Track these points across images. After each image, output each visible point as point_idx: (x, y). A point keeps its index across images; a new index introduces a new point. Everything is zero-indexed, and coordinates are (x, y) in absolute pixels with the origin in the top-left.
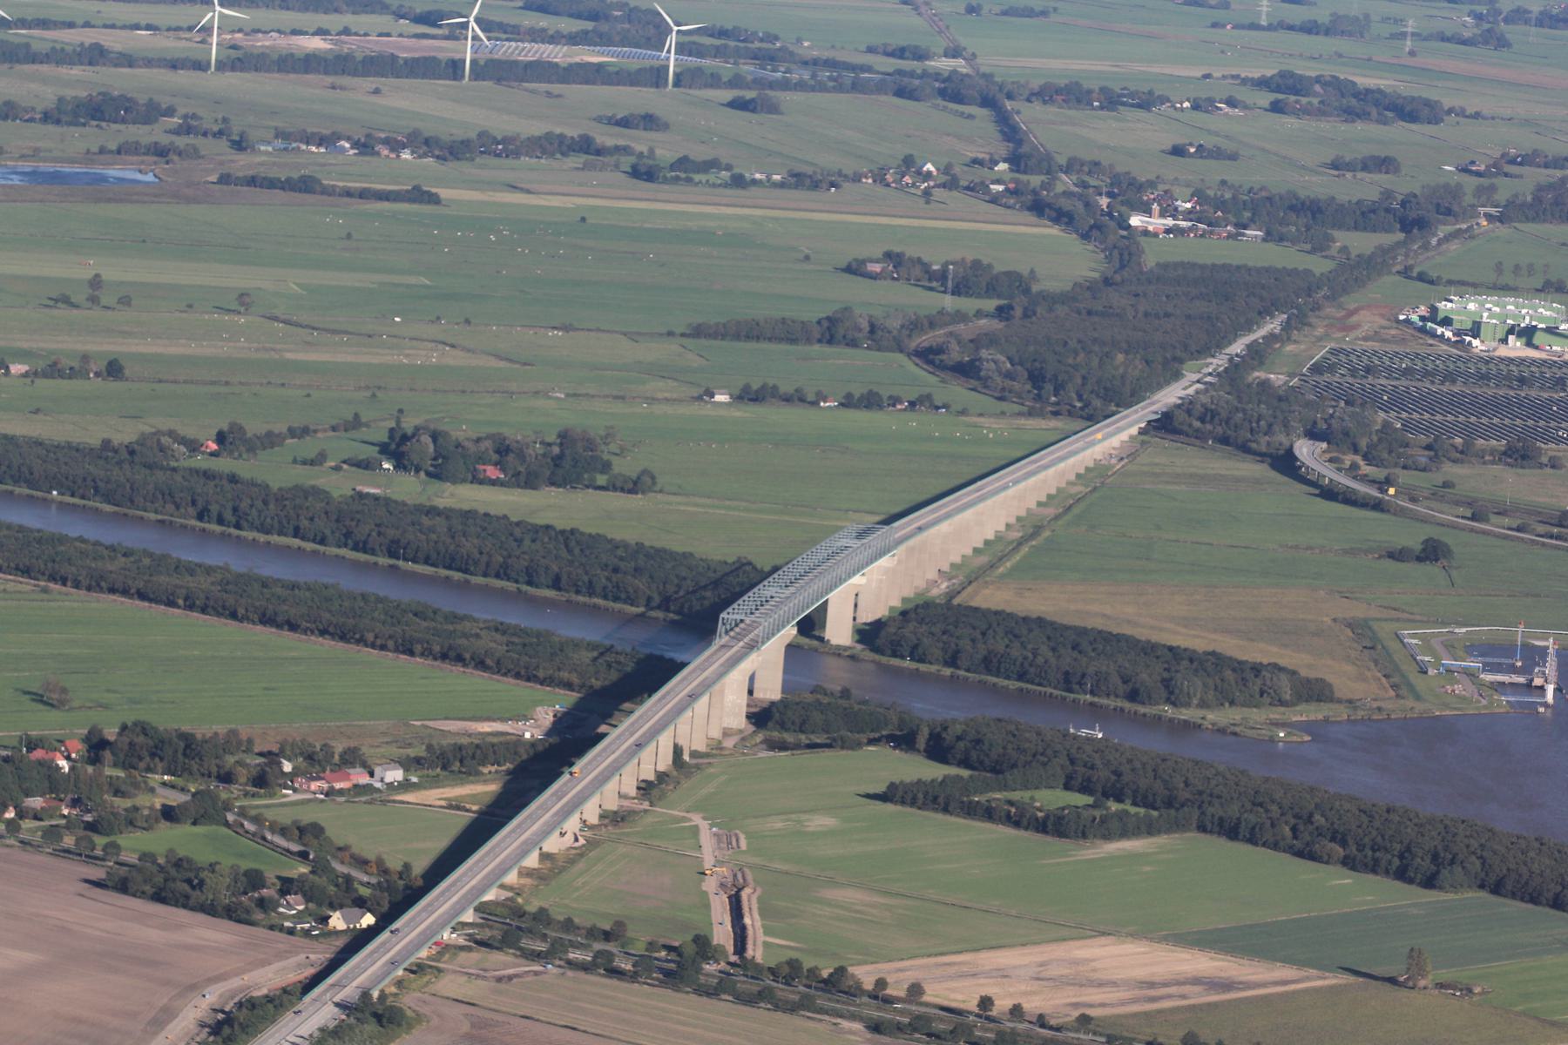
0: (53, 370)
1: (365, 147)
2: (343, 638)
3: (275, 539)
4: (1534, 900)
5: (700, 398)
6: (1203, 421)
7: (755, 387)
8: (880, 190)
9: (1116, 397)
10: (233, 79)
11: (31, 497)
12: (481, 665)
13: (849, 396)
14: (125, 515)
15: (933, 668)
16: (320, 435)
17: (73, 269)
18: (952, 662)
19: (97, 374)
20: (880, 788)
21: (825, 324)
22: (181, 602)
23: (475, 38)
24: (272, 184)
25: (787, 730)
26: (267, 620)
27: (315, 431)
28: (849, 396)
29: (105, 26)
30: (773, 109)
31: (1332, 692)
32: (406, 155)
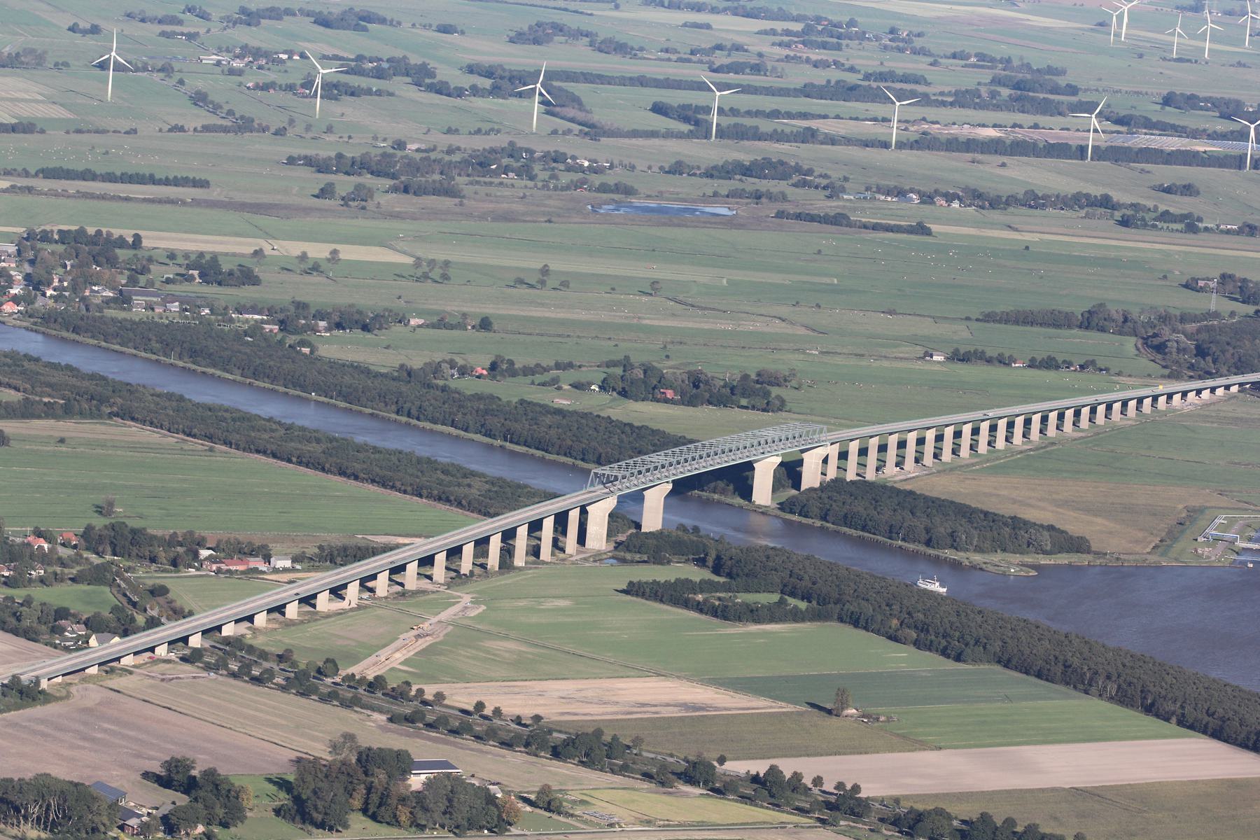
0: (441, 323)
1: (927, 199)
2: (384, 486)
3: (439, 427)
4: (1027, 673)
5: (923, 358)
7: (962, 351)
9: (1241, 367)
10: (905, 154)
11: (299, 397)
12: (460, 505)
13: (1033, 360)
14: (360, 412)
15: (810, 521)
17: (531, 262)
18: (824, 518)
19: (473, 327)
21: (1086, 315)
23: (541, 94)
24: (812, 218)
25: (630, 551)
26: (342, 473)
28: (1033, 360)
29: (851, 119)
31: (1089, 547)
32: (956, 204)
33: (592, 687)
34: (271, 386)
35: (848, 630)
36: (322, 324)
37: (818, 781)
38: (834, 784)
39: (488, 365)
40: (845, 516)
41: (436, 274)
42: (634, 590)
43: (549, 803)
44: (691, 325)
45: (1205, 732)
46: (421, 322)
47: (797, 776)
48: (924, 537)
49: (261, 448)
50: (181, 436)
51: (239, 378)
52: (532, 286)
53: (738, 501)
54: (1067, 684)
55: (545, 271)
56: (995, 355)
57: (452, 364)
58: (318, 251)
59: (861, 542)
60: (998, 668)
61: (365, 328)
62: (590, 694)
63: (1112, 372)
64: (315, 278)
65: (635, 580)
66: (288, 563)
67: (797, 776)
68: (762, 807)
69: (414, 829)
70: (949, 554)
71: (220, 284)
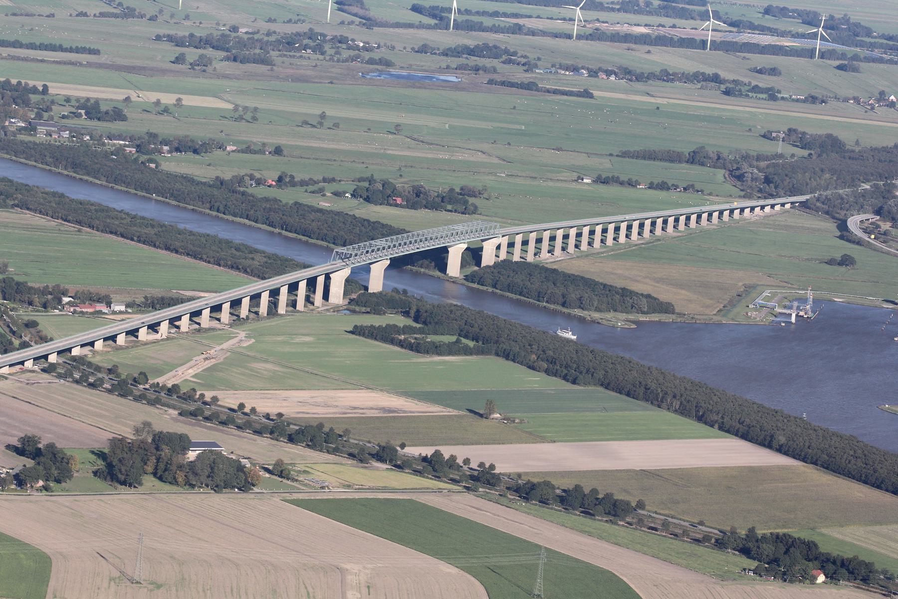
0: (248, 150)
1: (593, 73)
2: (195, 258)
3: (238, 219)
4: (620, 393)
6: (823, 203)
7: (604, 176)
8: (857, 107)
9: (793, 192)
10: (582, 43)
11: (144, 196)
12: (246, 272)
14: (185, 208)
15: (485, 288)
18: (494, 286)
19: (270, 153)
21: (692, 154)
24: (512, 85)
26: (167, 248)
30: (856, 70)
31: (674, 309)
32: (613, 78)
34: (126, 189)
35: (501, 361)
36: (166, 148)
37: (467, 461)
40: (509, 285)
41: (248, 116)
42: (357, 331)
43: (282, 472)
46: (234, 148)
47: (453, 458)
48: (561, 300)
49: (114, 230)
50: (60, 221)
51: (104, 183)
52: (314, 126)
53: (437, 273)
55: (323, 116)
56: (626, 180)
57: (252, 177)
58: (168, 99)
59: (518, 303)
60: (601, 389)
61: (195, 151)
62: (319, 400)
63: (705, 193)
64: (166, 117)
66: (123, 308)
67: (453, 458)
68: (428, 478)
69: (187, 487)
70: (577, 312)
71: (99, 119)
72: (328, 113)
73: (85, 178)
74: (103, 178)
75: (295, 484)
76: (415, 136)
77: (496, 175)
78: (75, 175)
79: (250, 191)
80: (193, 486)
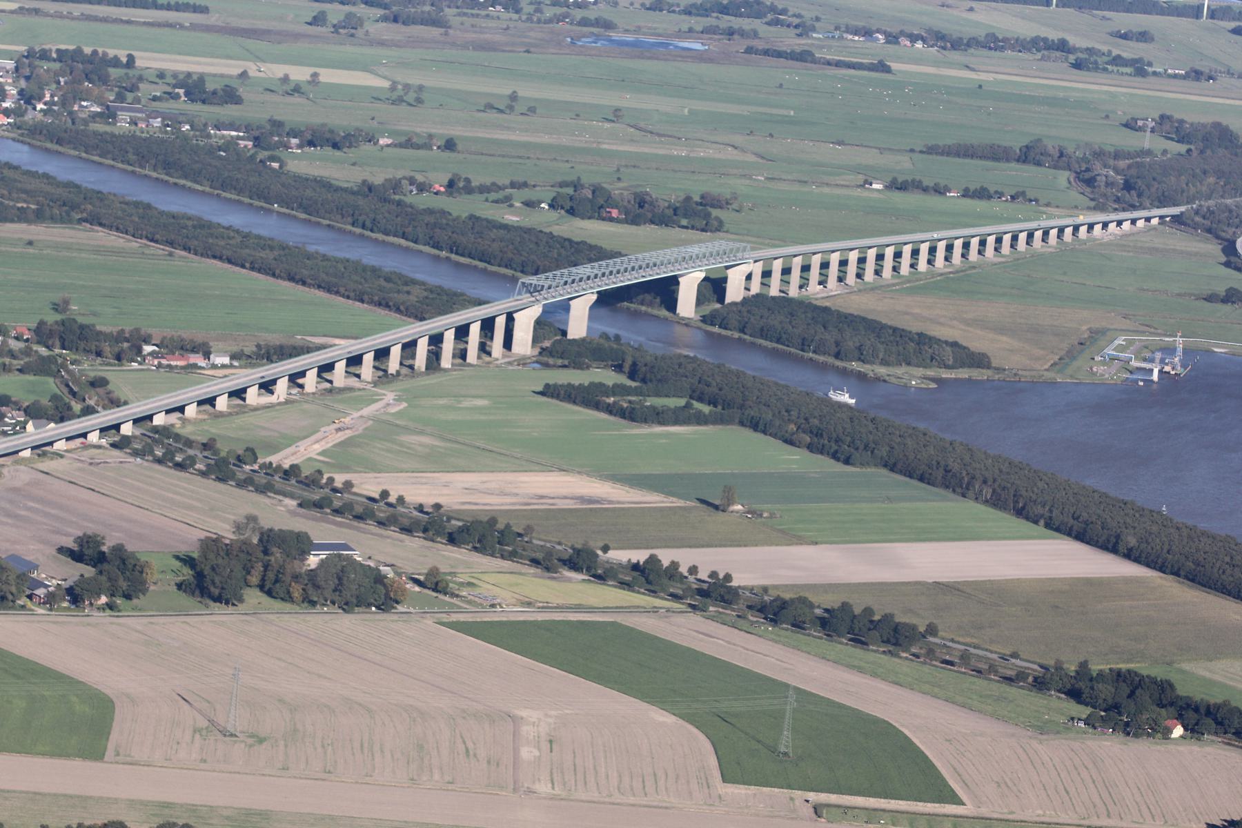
0: (409, 144)
1: (892, 39)
2: (329, 291)
4: (911, 477)
5: (862, 186)
6: (1204, 218)
7: (900, 180)
9: (1163, 201)
12: (398, 310)
15: (729, 333)
16: (538, 188)
17: (501, 88)
19: (439, 148)
20: (540, 389)
22: (247, 265)
24: (779, 54)
26: (291, 279)
27: (534, 186)
31: (989, 362)
32: (919, 45)
33: (495, 480)
34: (237, 198)
35: (747, 433)
36: (294, 141)
37: (693, 570)
38: (708, 573)
39: (446, 182)
41: (411, 97)
42: (549, 391)
43: (437, 584)
44: (646, 150)
45: (1069, 534)
46: (389, 141)
47: (674, 565)
48: (834, 349)
50: (144, 241)
51: (208, 189)
53: (664, 313)
54: (947, 487)
55: (514, 97)
56: (932, 185)
57: (412, 181)
58: (300, 74)
59: (775, 354)
60: (885, 471)
61: (336, 146)
64: (296, 99)
65: (551, 382)
66: (226, 360)
67: (674, 565)
68: (639, 592)
69: (306, 604)
71: (204, 102)
72: (520, 94)
73: (182, 182)
74: (206, 182)
75: (454, 600)
76: (642, 124)
77: (750, 178)
78: (167, 178)
79: (408, 199)
80: (313, 603)
